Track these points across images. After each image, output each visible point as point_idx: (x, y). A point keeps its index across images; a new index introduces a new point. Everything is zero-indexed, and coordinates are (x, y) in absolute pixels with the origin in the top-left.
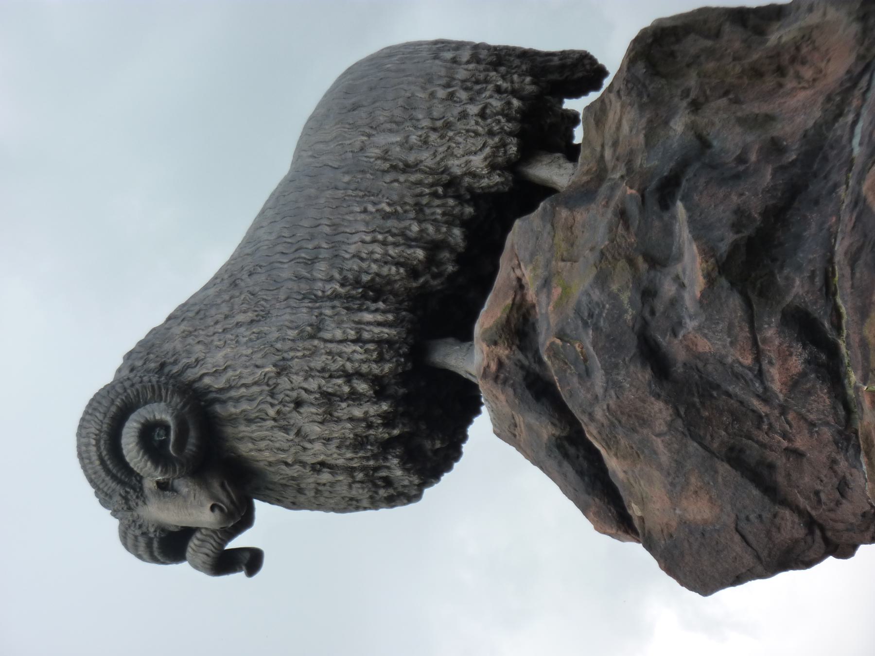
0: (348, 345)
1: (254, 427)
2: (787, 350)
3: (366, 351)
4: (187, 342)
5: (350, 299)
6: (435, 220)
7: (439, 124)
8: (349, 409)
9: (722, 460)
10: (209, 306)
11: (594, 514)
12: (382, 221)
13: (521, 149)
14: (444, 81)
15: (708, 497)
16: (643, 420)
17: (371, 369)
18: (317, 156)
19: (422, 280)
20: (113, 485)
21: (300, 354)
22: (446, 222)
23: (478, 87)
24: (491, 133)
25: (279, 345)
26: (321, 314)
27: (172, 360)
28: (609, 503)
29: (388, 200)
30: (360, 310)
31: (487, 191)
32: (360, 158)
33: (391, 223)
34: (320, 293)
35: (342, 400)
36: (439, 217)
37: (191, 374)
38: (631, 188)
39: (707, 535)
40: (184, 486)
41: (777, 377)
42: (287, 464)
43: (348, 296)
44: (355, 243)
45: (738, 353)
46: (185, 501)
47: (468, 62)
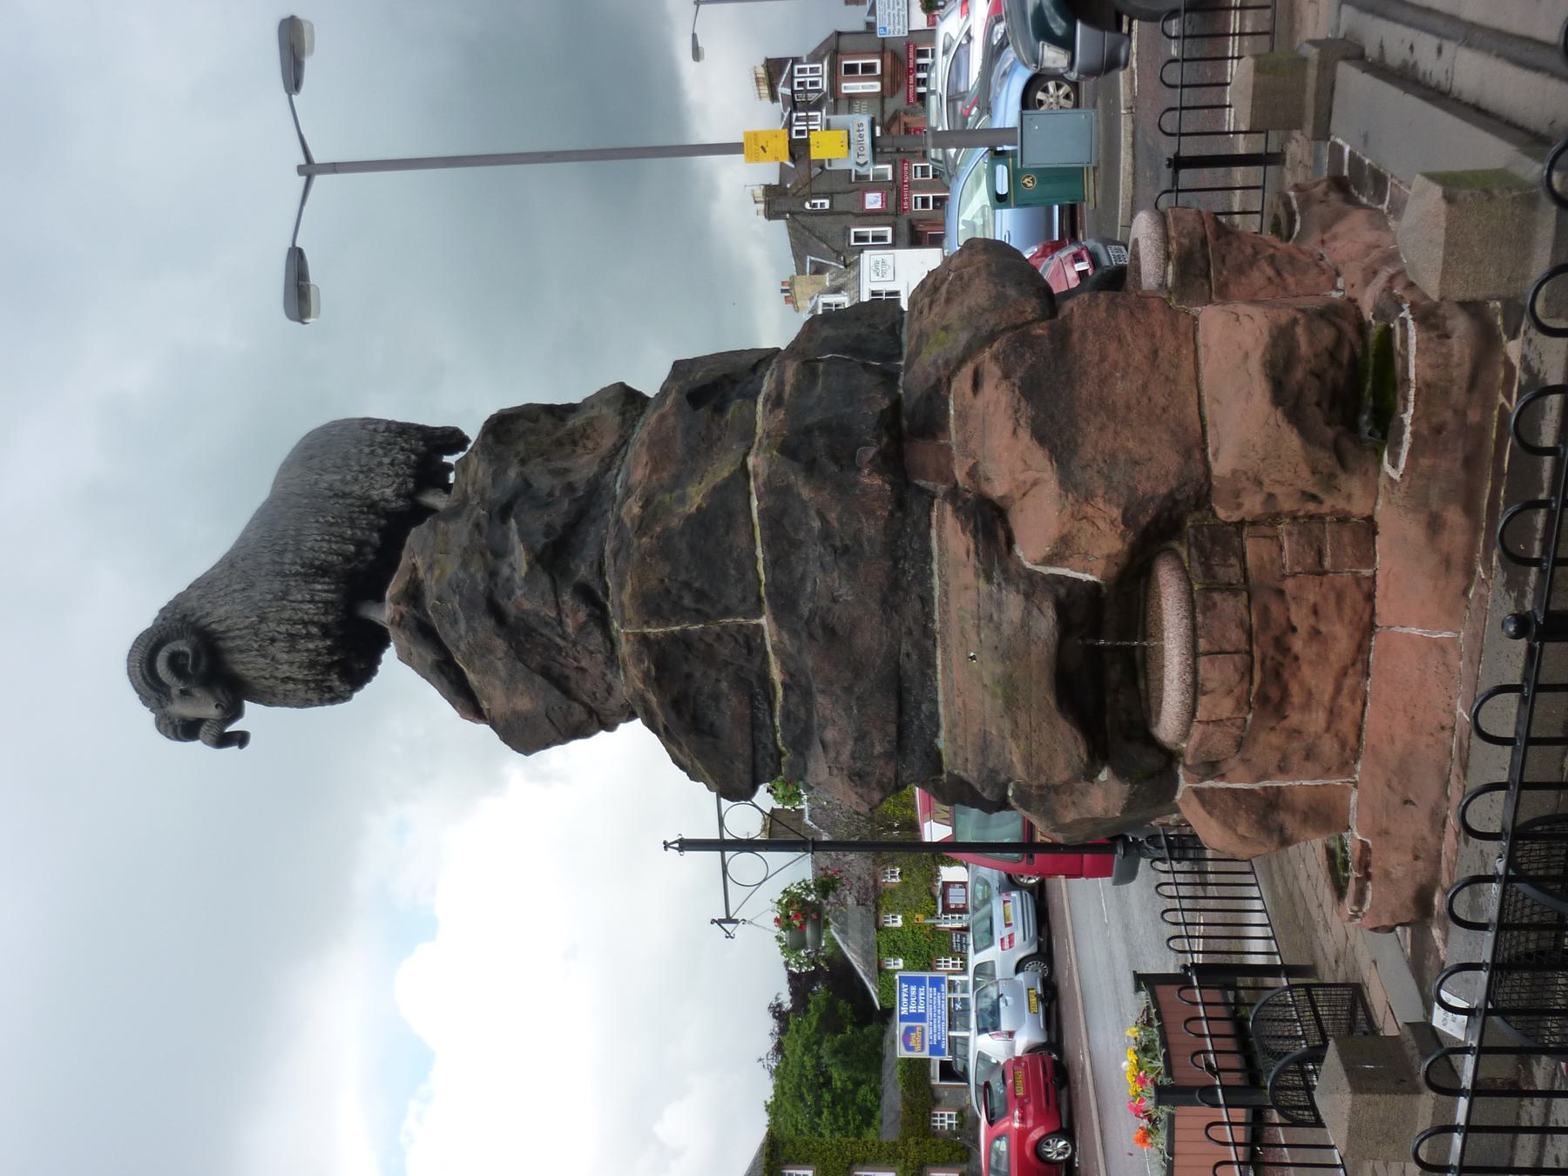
19: (353, 565)
24: (397, 475)
37: (204, 622)
42: (265, 678)
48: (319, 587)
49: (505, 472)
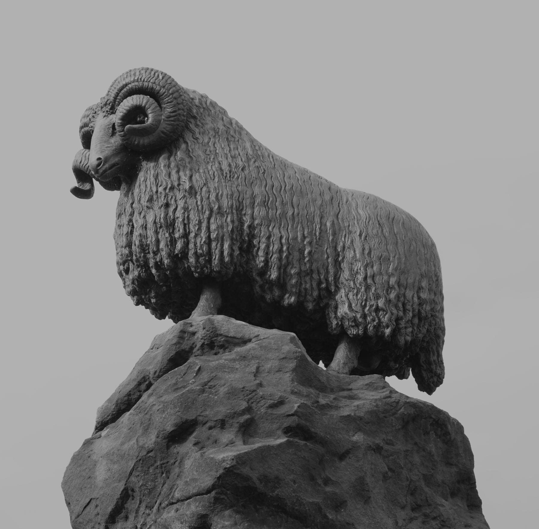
0: (207, 234)
1: (152, 179)
2: (184, 520)
3: (201, 246)
4: (210, 131)
5: (240, 232)
6: (301, 284)
7: (369, 281)
8: (165, 238)
9: (125, 485)
10: (237, 143)
11: (107, 405)
12: (297, 249)
13: (356, 336)
14: (403, 281)
15: (107, 478)
16: (147, 429)
17: (191, 250)
18: (347, 204)
19: (258, 278)
20: (113, 95)
21: (199, 203)
22: (300, 291)
23: (400, 305)
24: (364, 316)
25: (204, 189)
26: (228, 214)
27: (198, 123)
28: (113, 415)
29: (313, 251)
30: (232, 239)
31: (327, 317)
32: (344, 231)
33: (296, 254)
34: (244, 212)
35: (170, 234)
36: (303, 286)
37: (189, 137)
38: (299, 407)
39: (89, 480)
40: (116, 140)
41: (170, 515)
42: (132, 204)
43: (243, 231)
44: (280, 232)
45: (181, 487)
46: (105, 142)
47: (419, 298)
48: (226, 246)
49: (359, 429)
